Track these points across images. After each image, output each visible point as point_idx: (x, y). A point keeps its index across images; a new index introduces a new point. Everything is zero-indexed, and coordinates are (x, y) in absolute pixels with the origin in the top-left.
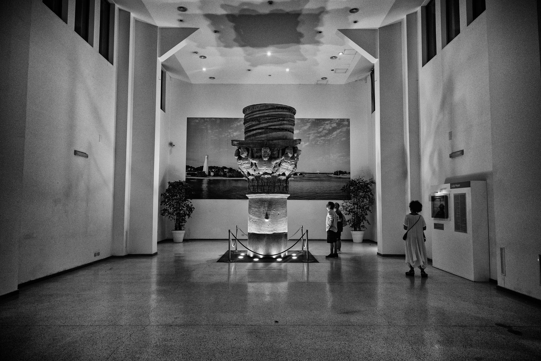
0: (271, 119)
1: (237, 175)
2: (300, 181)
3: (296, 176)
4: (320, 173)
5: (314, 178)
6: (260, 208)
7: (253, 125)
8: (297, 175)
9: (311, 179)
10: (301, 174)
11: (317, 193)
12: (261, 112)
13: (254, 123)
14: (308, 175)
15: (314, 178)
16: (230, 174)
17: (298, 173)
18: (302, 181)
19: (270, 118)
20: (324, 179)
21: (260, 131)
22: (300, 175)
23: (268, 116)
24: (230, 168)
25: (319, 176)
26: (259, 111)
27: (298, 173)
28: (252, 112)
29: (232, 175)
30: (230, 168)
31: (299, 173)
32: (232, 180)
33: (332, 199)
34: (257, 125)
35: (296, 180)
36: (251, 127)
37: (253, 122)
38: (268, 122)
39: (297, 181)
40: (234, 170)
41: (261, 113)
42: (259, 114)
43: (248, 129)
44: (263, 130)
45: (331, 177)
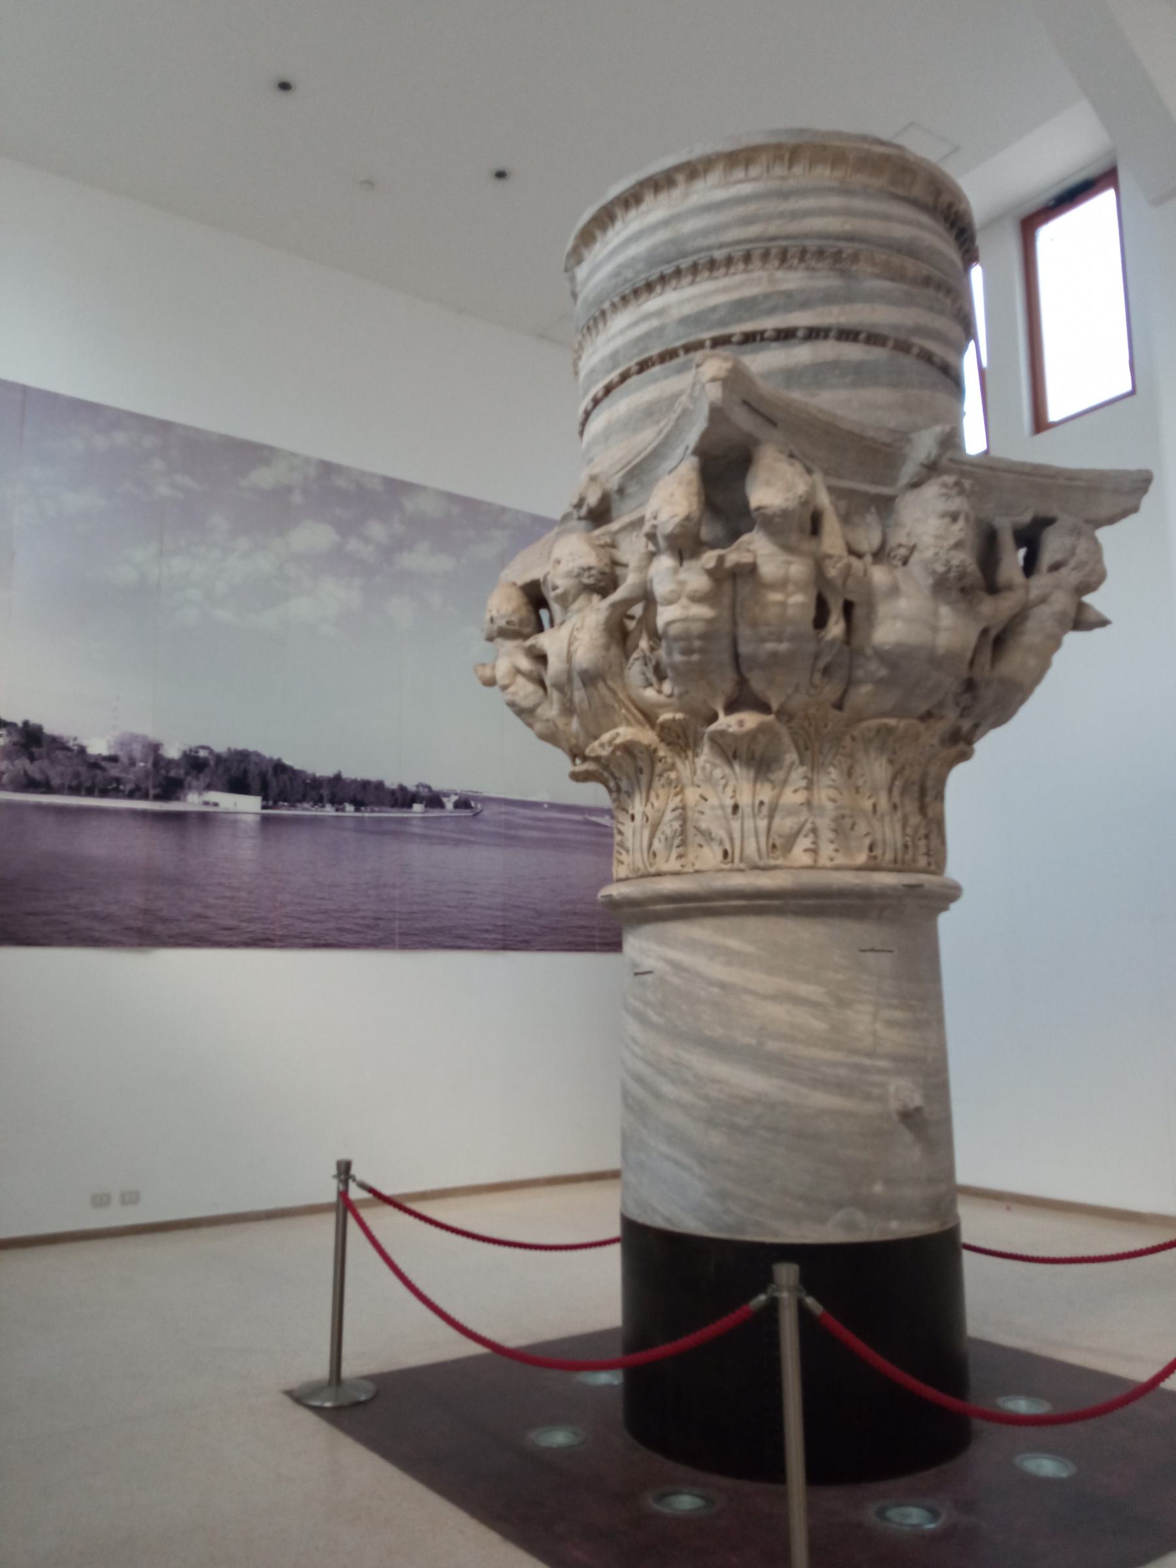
0: (927, 281)
1: (77, 775)
2: (458, 842)
3: (435, 813)
4: (553, 806)
5: (526, 827)
6: (842, 1003)
7: (788, 294)
8: (441, 805)
9: (512, 832)
10: (463, 803)
11: (540, 914)
12: (858, 203)
13: (793, 280)
14: (495, 808)
15: (526, 827)
16: (23, 764)
17: (447, 795)
18: (469, 842)
19: (925, 269)
20: (571, 837)
21: (853, 352)
22: (457, 805)
23: (910, 250)
24: (26, 724)
25: (549, 820)
26: (845, 191)
27: (447, 795)
28: (784, 195)
29: (38, 776)
30: (26, 724)
31: (454, 798)
32: (39, 807)
33: (608, 944)
34: (828, 298)
35: (438, 833)
36: (771, 311)
37: (780, 274)
38: (909, 301)
39: (443, 841)
40: (57, 743)
41: (866, 215)
42: (847, 212)
43: (722, 323)
44: (876, 354)
45: (603, 830)
